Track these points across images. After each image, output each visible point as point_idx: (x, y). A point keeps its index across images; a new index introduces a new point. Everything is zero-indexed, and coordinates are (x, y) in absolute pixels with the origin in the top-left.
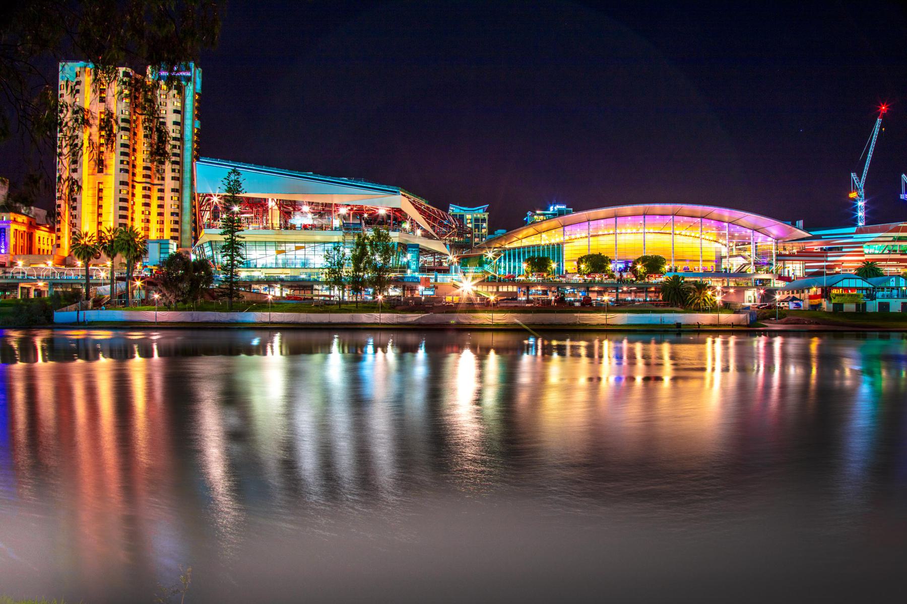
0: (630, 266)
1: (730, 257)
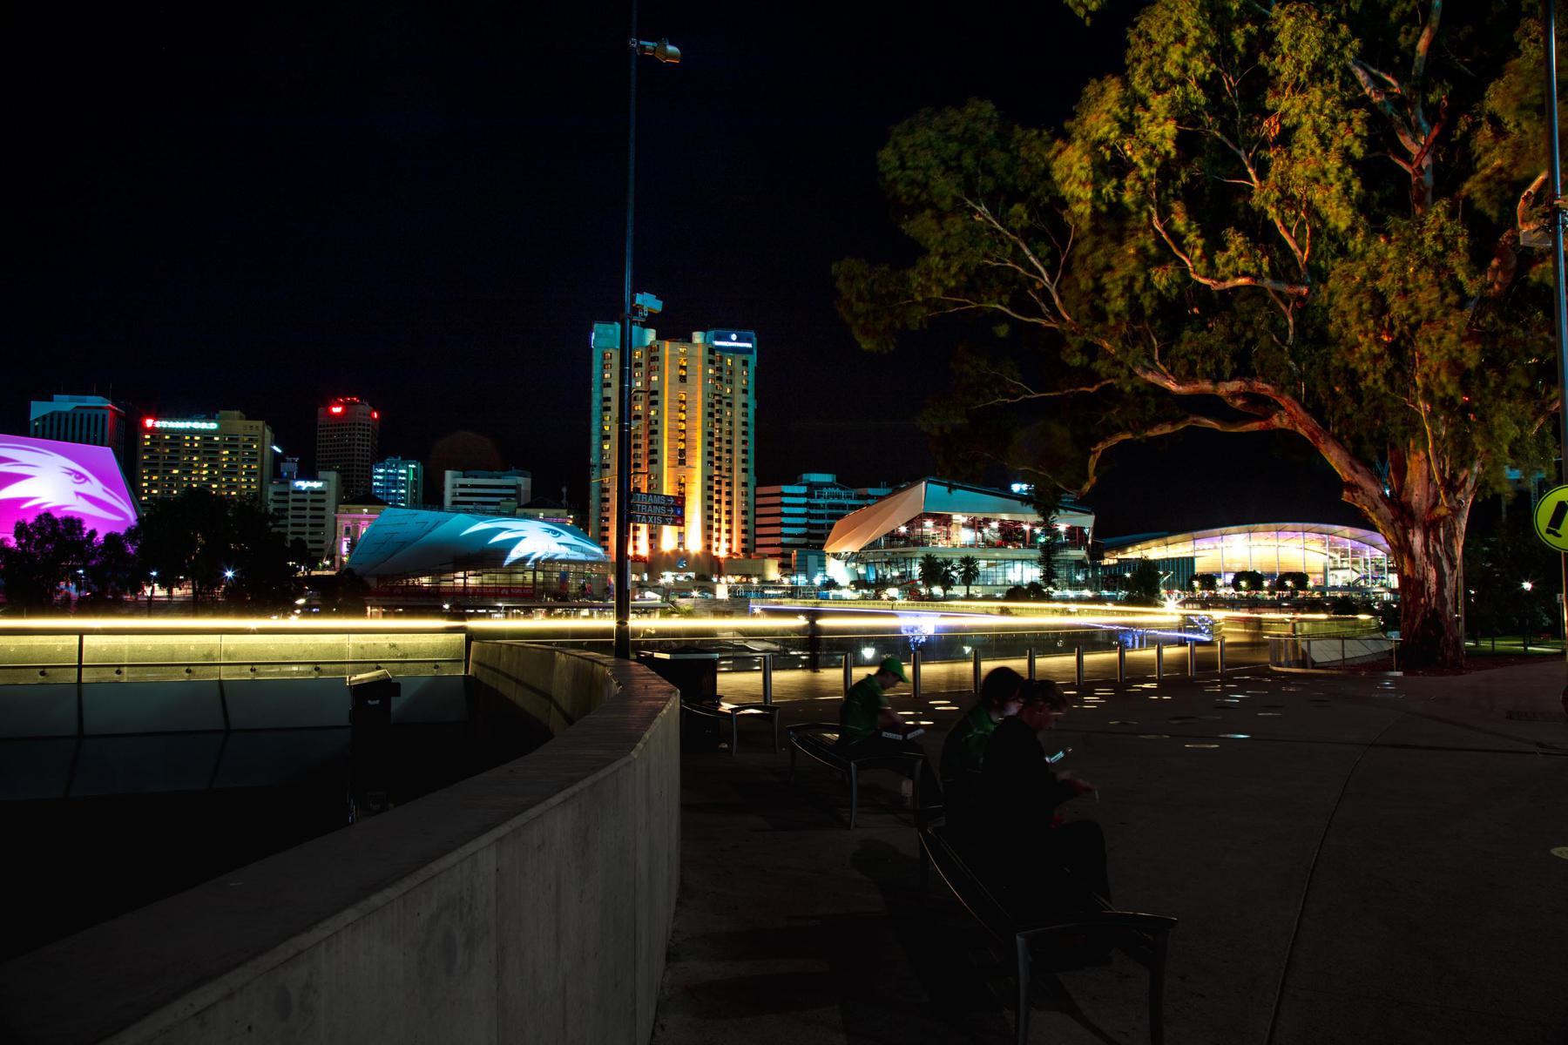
0: (1279, 583)
1: (1335, 569)
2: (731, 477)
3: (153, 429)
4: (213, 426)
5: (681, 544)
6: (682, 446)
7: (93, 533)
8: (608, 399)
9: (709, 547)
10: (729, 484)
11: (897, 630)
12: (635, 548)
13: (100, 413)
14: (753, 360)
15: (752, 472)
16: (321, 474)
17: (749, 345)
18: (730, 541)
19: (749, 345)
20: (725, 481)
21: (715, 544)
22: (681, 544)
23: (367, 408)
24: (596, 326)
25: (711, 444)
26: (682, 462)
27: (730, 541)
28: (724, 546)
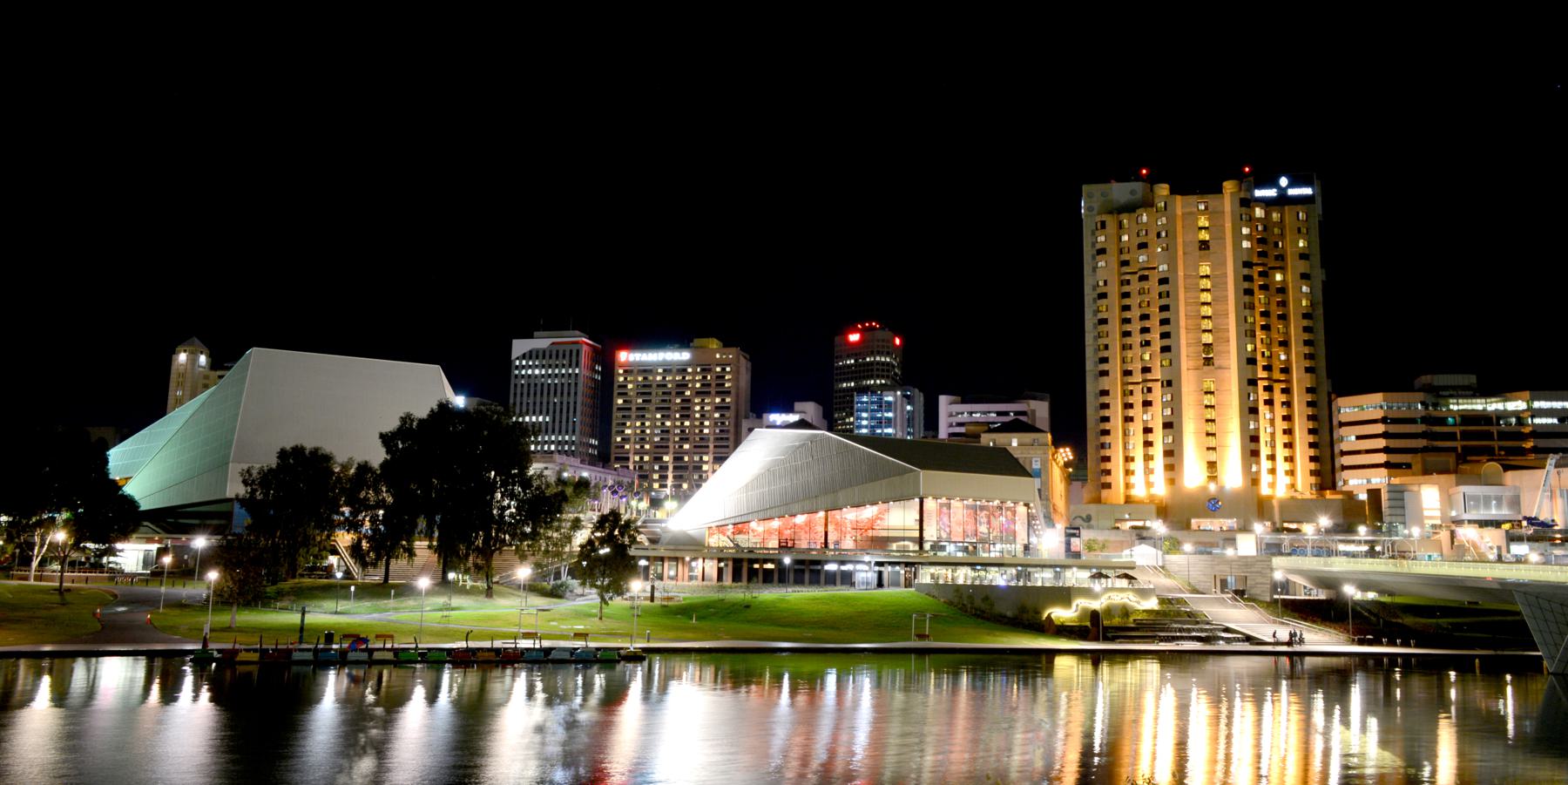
2: (1288, 381)
3: (627, 364)
4: (684, 356)
5: (1213, 478)
6: (1207, 338)
7: (345, 467)
8: (1105, 393)
9: (1255, 481)
10: (1286, 391)
11: (318, 700)
12: (1128, 486)
13: (575, 348)
14: (1318, 207)
15: (1323, 372)
16: (798, 406)
17: (1308, 191)
18: (1291, 473)
19: (1308, 191)
20: (1278, 387)
21: (1265, 478)
22: (1213, 478)
23: (887, 334)
24: (1085, 188)
25: (1164, 322)
26: (1208, 361)
27: (1291, 473)
28: (1283, 480)
